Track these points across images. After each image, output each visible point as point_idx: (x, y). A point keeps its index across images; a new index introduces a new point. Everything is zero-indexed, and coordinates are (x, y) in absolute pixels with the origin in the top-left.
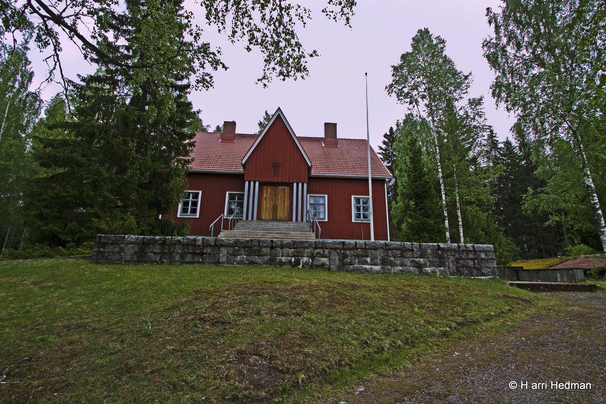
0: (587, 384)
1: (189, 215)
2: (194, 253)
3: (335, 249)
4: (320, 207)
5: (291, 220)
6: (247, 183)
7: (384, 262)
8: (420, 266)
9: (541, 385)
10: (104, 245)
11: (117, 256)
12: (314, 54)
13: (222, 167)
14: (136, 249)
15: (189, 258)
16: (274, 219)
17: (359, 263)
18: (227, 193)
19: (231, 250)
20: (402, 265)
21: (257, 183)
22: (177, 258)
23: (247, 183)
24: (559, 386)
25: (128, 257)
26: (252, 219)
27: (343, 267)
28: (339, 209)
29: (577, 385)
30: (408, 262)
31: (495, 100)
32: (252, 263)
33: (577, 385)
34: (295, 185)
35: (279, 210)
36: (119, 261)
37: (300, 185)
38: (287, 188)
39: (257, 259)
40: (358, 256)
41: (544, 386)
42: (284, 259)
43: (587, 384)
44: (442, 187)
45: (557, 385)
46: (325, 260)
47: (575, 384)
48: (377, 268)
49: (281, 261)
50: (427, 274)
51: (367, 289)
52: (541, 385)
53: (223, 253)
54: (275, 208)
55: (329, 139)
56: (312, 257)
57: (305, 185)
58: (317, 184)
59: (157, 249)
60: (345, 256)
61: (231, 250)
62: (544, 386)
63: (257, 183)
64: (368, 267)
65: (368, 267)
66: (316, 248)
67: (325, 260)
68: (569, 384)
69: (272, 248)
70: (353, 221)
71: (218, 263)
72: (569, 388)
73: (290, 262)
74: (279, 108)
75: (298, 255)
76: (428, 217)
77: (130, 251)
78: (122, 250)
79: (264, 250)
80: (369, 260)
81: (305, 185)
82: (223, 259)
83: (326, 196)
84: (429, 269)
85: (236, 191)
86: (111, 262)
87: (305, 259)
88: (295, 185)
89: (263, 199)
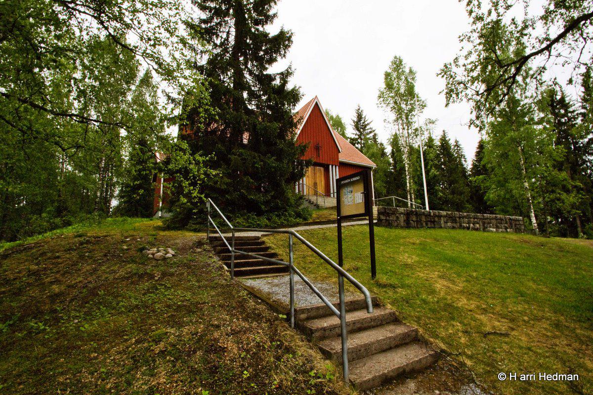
0: (574, 376)
9: (529, 377)
13: (320, 134)
22: (424, 224)
24: (547, 377)
27: (485, 230)
29: (564, 377)
31: (361, 109)
33: (564, 377)
34: (331, 166)
41: (532, 377)
43: (574, 376)
45: (545, 376)
47: (563, 376)
51: (135, 279)
52: (529, 377)
62: (532, 377)
68: (557, 376)
72: (557, 379)
74: (316, 97)
81: (337, 167)
88: (331, 166)
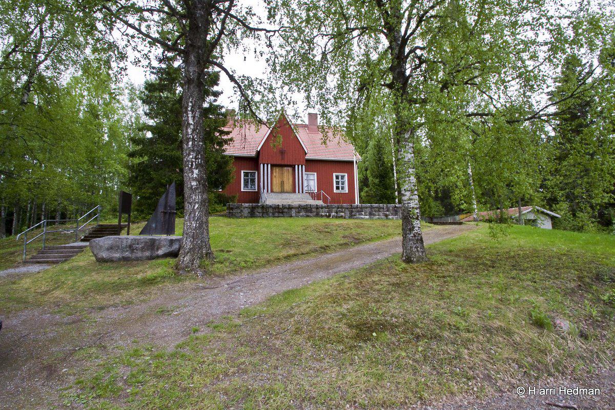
1: (340, 191)
2: (279, 212)
3: (348, 208)
4: (311, 181)
5: (294, 191)
6: (262, 165)
7: (370, 214)
8: (386, 216)
10: (232, 209)
11: (240, 214)
12: (477, 225)
14: (249, 210)
15: (276, 214)
16: (282, 192)
17: (359, 214)
18: (242, 172)
19: (297, 210)
20: (379, 215)
21: (269, 166)
23: (262, 165)
25: (246, 215)
26: (268, 191)
27: (351, 216)
28: (324, 184)
30: (381, 214)
32: (308, 216)
34: (296, 166)
35: (285, 185)
36: (241, 217)
37: (300, 166)
38: (290, 169)
39: (310, 214)
40: (358, 211)
42: (323, 214)
44: (395, 168)
46: (343, 214)
48: (367, 217)
49: (322, 215)
50: (390, 219)
53: (293, 212)
54: (282, 183)
55: (311, 127)
56: (337, 212)
57: (304, 166)
58: (312, 164)
59: (260, 210)
60: (352, 212)
61: (297, 210)
63: (269, 166)
64: (363, 217)
65: (363, 217)
66: (338, 208)
67: (343, 214)
69: (317, 208)
70: (242, 190)
71: (291, 216)
73: (326, 215)
75: (330, 212)
76: (387, 189)
77: (246, 212)
78: (242, 211)
79: (313, 209)
80: (363, 213)
81: (304, 166)
82: (294, 215)
83: (316, 174)
84: (390, 217)
85: (249, 170)
86: (238, 217)
87: (333, 214)
88: (296, 166)
89: (274, 176)
